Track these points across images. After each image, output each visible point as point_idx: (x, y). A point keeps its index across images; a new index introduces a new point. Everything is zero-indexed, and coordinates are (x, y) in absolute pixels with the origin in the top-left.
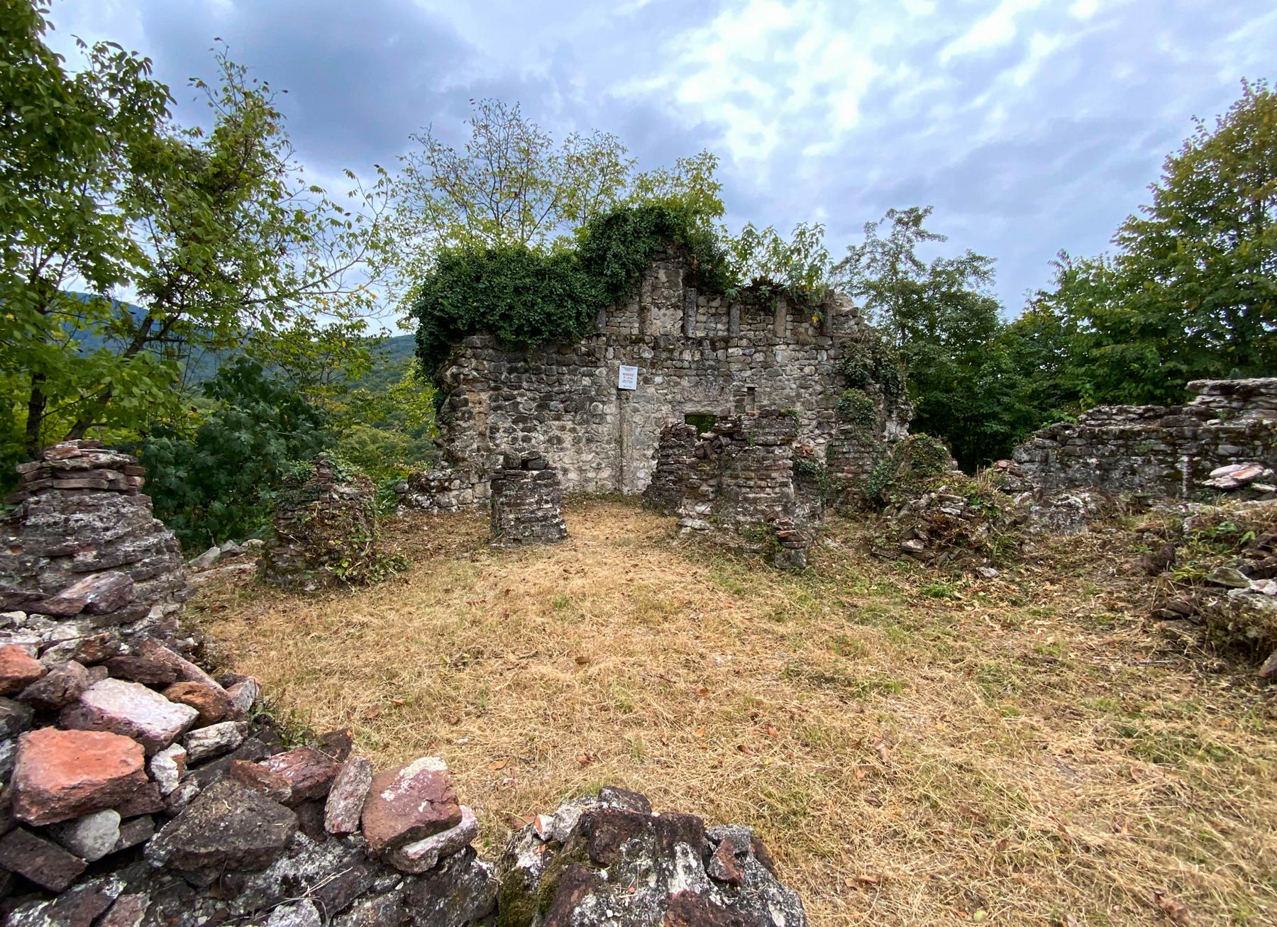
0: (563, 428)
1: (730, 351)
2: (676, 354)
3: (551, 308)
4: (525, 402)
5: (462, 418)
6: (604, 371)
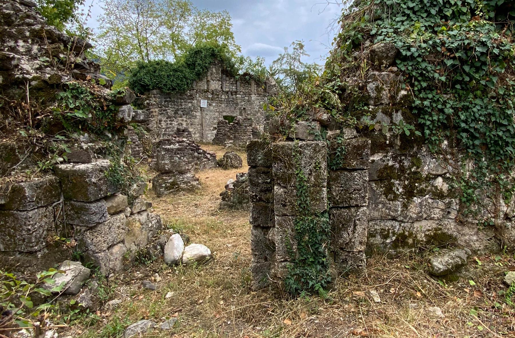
0: (183, 120)
2: (220, 96)
3: (179, 82)
4: (170, 112)
5: (151, 117)
6: (196, 101)
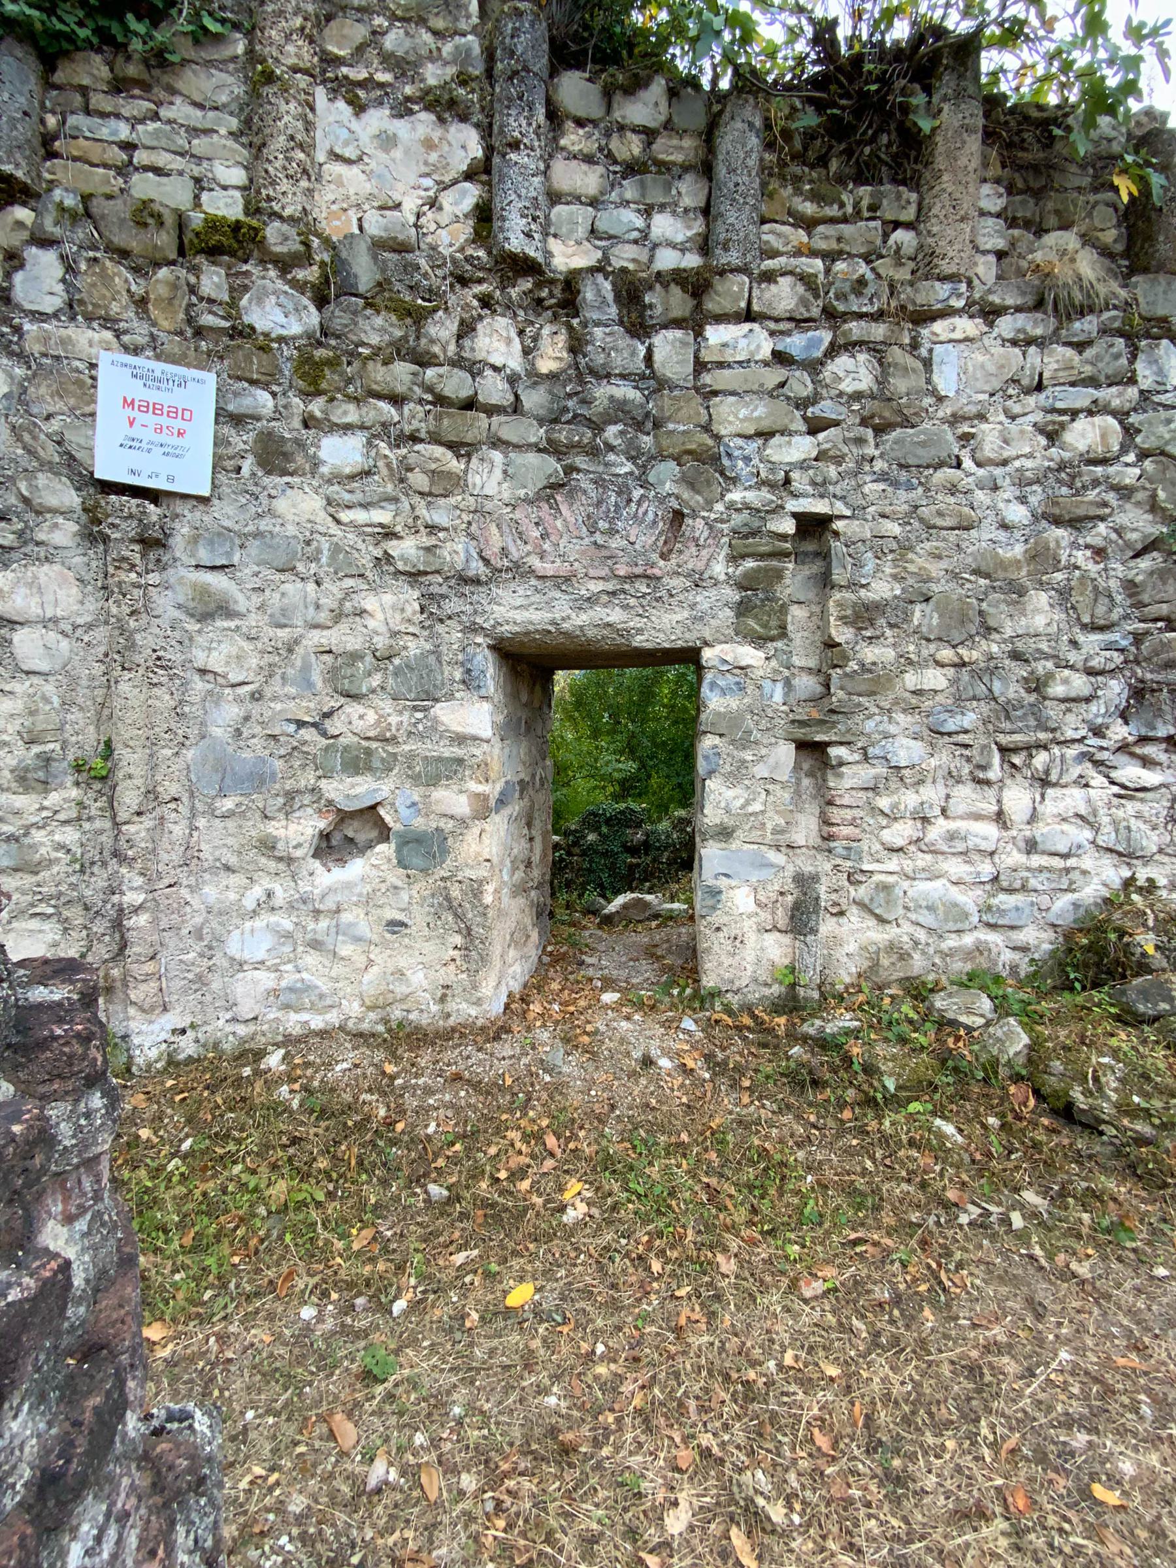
1: (715, 334)
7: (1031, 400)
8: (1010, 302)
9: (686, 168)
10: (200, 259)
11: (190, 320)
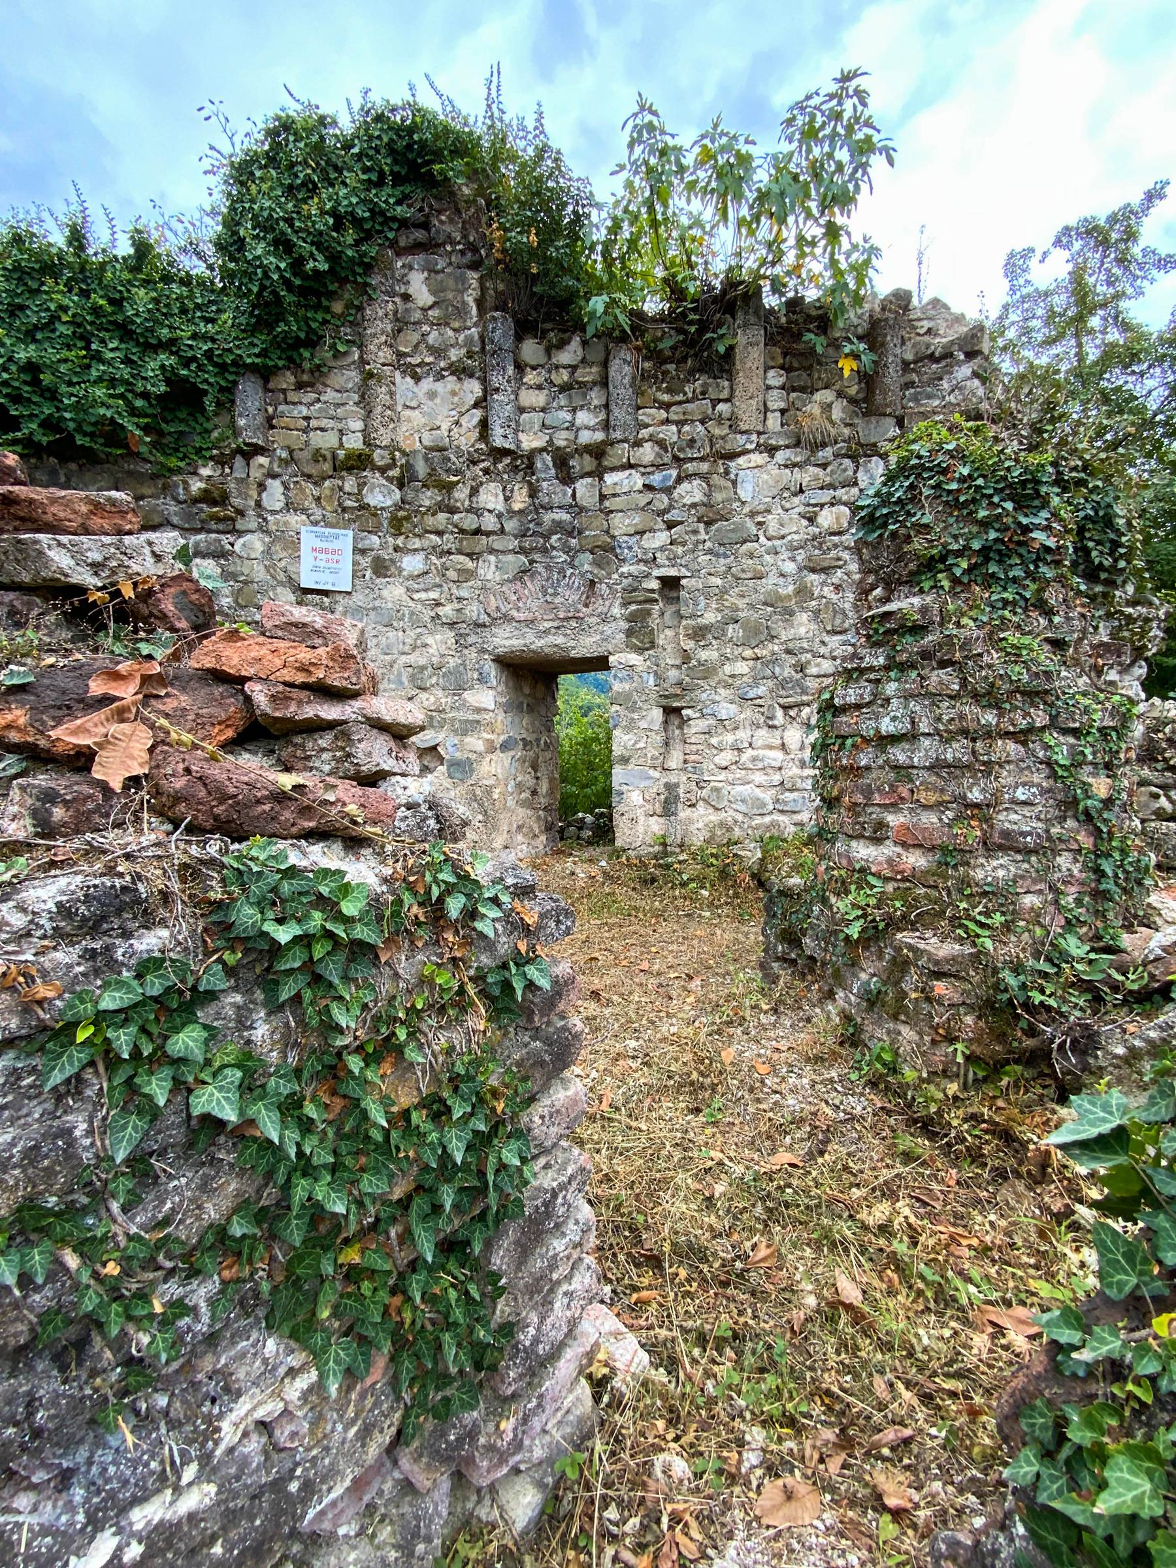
1: (610, 478)
2: (461, 494)
7: (796, 500)
8: (781, 443)
9: (594, 383)
10: (344, 473)
11: (340, 504)
